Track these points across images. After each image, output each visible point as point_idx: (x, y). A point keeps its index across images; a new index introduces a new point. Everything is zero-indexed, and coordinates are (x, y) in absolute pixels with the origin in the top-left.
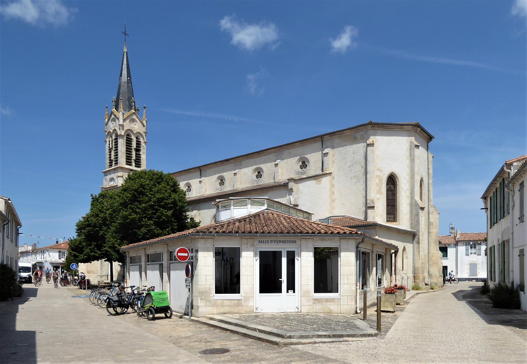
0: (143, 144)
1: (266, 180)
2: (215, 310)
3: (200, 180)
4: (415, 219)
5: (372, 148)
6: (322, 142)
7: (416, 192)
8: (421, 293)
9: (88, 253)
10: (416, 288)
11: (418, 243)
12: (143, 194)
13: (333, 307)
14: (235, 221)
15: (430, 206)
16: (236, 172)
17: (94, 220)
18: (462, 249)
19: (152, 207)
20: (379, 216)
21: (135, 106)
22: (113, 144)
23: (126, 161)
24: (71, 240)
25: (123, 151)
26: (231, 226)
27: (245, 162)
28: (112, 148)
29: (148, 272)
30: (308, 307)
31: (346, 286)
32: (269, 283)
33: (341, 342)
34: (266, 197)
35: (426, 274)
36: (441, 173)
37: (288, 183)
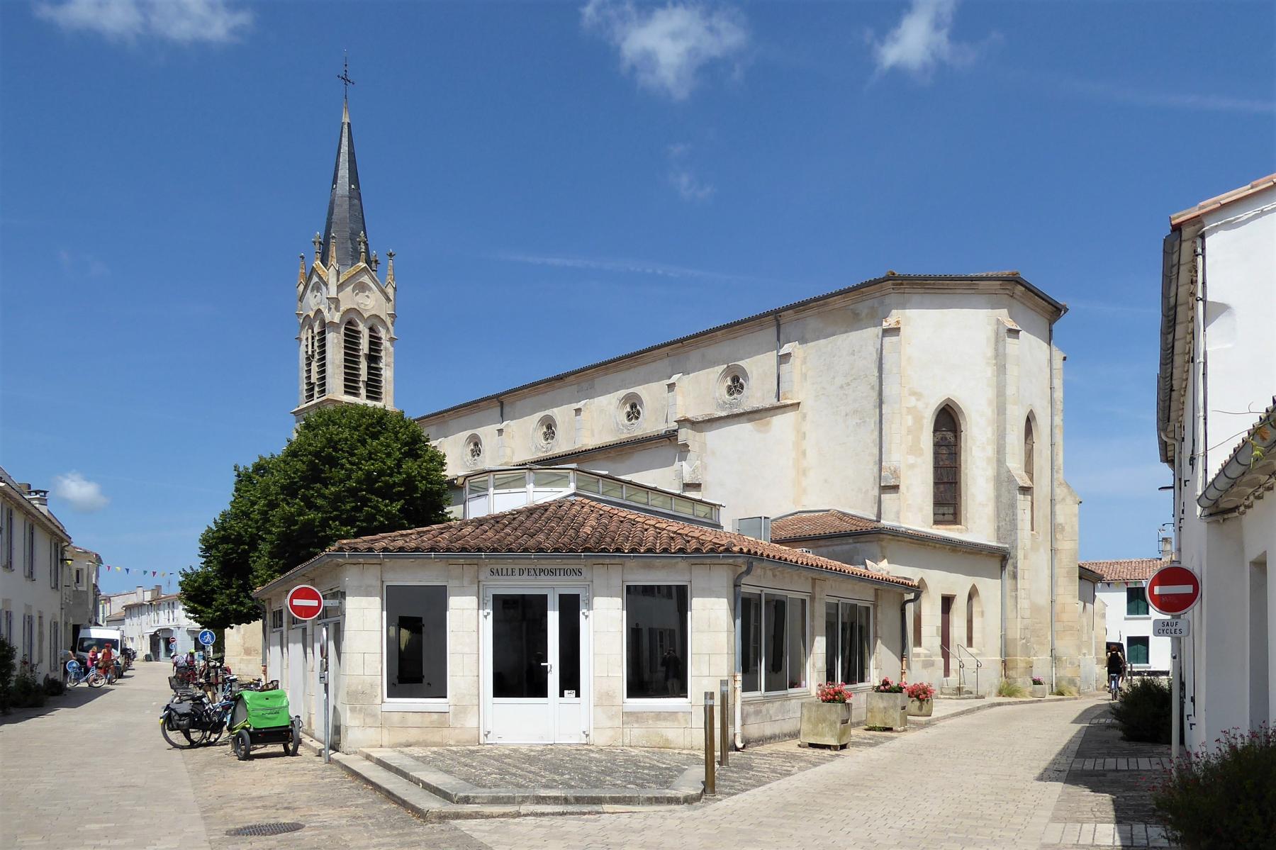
0: (386, 344)
2: (386, 737)
3: (499, 426)
4: (1006, 518)
5: (894, 339)
6: (779, 326)
7: (1008, 449)
8: (1009, 704)
10: (1008, 691)
11: (1015, 577)
15: (1055, 484)
17: (237, 526)
19: (353, 492)
20: (913, 511)
22: (316, 344)
23: (346, 386)
24: (186, 575)
25: (337, 362)
28: (313, 356)
32: (518, 675)
33: (584, 814)
34: (574, 466)
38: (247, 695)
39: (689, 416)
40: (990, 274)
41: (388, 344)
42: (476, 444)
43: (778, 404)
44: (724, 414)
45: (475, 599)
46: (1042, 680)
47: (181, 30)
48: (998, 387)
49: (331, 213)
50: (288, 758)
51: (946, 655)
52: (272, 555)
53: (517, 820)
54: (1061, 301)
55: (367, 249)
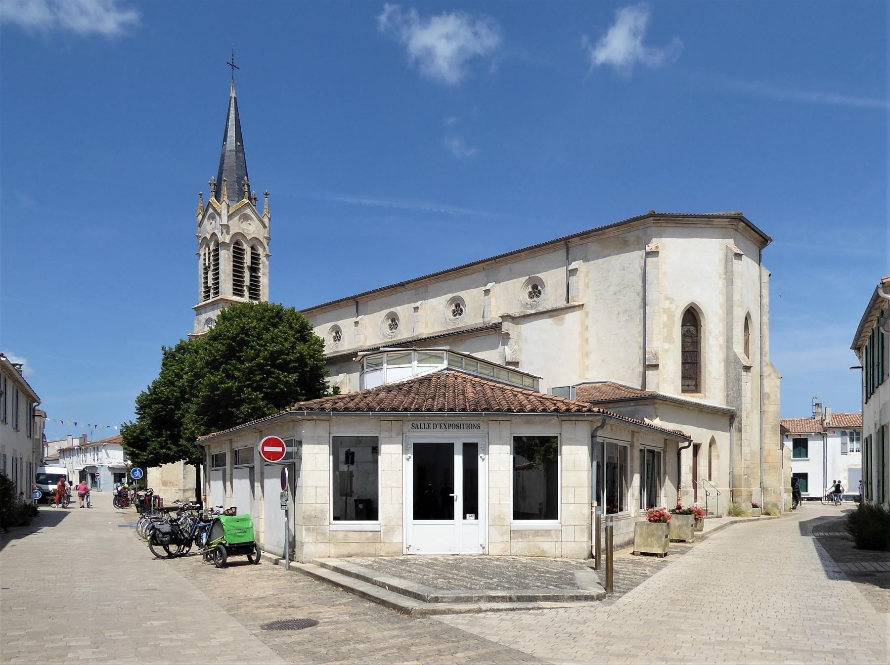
1: (470, 319)
2: (333, 550)
3: (355, 320)
4: (734, 388)
5: (654, 259)
6: (568, 249)
7: (735, 339)
8: (741, 521)
9: (155, 449)
10: (735, 512)
11: (740, 430)
12: (243, 343)
13: (548, 546)
14: (389, 389)
15: (764, 364)
16: (416, 305)
17: (166, 391)
18: (834, 442)
19: (260, 366)
20: (667, 382)
21: (249, 192)
22: (212, 258)
24: (127, 427)
25: (228, 272)
26: (370, 399)
27: (433, 287)
28: (209, 267)
29: (265, 480)
30: (501, 545)
31: (572, 507)
32: (432, 502)
33: (529, 609)
34: (447, 348)
35: (756, 488)
36: (783, 302)
37: (500, 323)
38: (223, 519)
39: (510, 313)
40: (721, 214)
41: (265, 259)
42: (337, 333)
43: (569, 305)
44: (533, 312)
45: (400, 446)
46: (758, 504)
47: (81, 24)
48: (727, 295)
49: (222, 163)
50: (253, 566)
51: (695, 486)
52: (198, 413)
53: (481, 615)
54: (768, 233)
55: (249, 189)
